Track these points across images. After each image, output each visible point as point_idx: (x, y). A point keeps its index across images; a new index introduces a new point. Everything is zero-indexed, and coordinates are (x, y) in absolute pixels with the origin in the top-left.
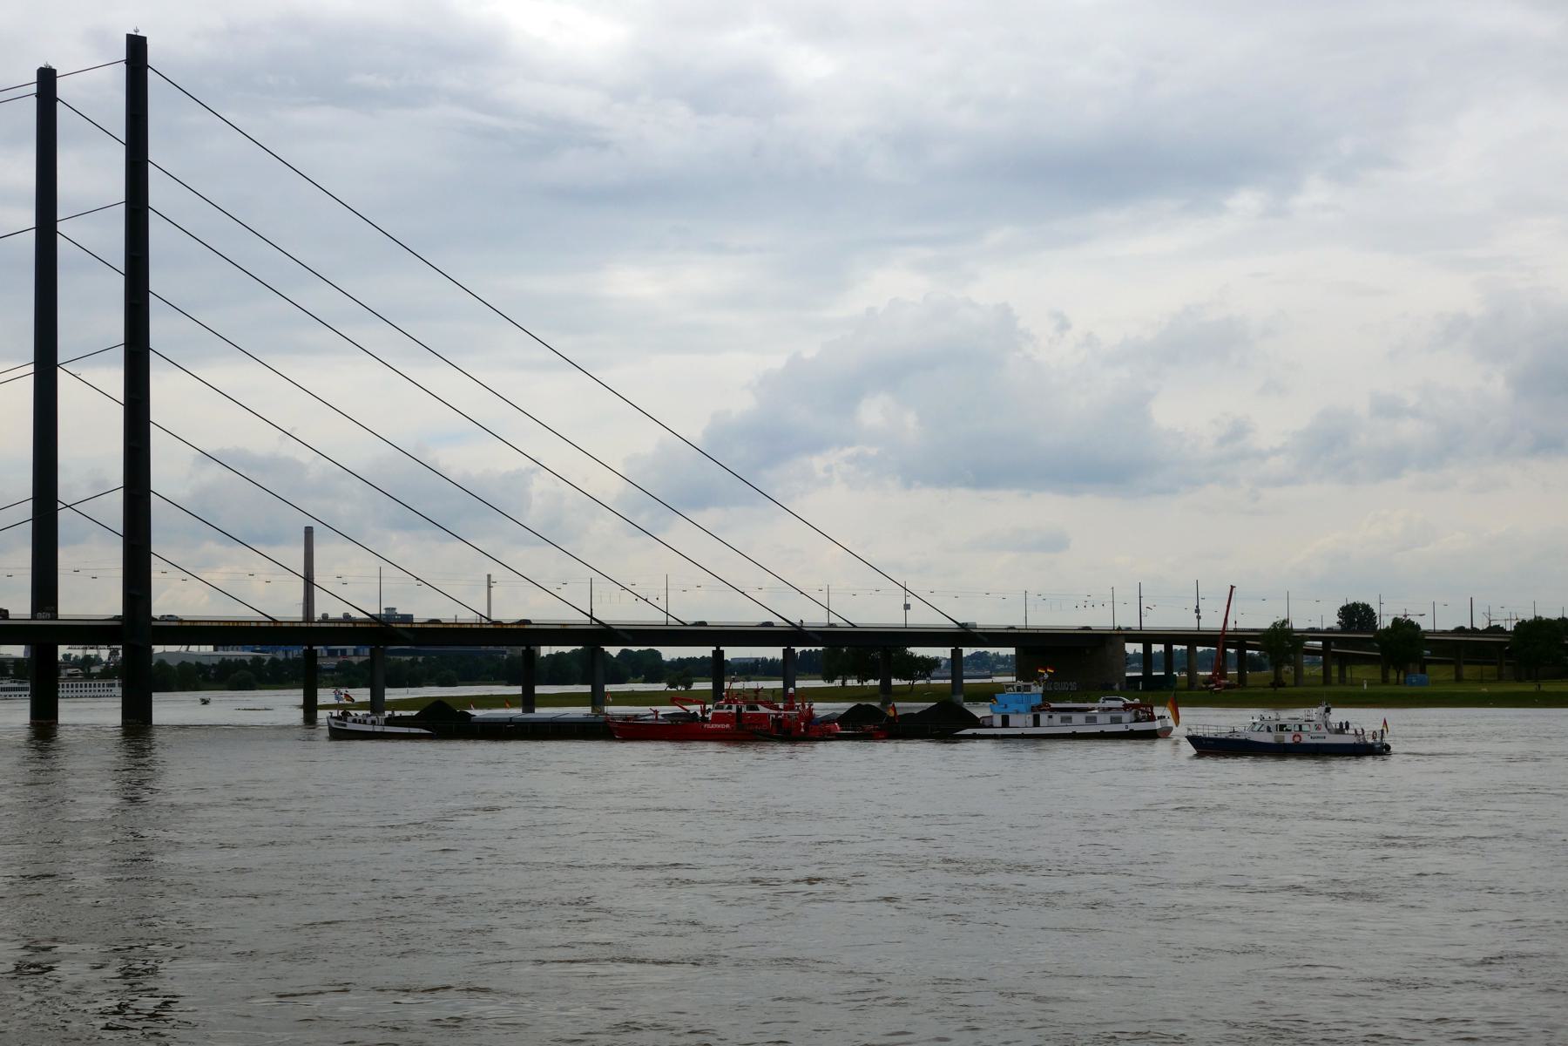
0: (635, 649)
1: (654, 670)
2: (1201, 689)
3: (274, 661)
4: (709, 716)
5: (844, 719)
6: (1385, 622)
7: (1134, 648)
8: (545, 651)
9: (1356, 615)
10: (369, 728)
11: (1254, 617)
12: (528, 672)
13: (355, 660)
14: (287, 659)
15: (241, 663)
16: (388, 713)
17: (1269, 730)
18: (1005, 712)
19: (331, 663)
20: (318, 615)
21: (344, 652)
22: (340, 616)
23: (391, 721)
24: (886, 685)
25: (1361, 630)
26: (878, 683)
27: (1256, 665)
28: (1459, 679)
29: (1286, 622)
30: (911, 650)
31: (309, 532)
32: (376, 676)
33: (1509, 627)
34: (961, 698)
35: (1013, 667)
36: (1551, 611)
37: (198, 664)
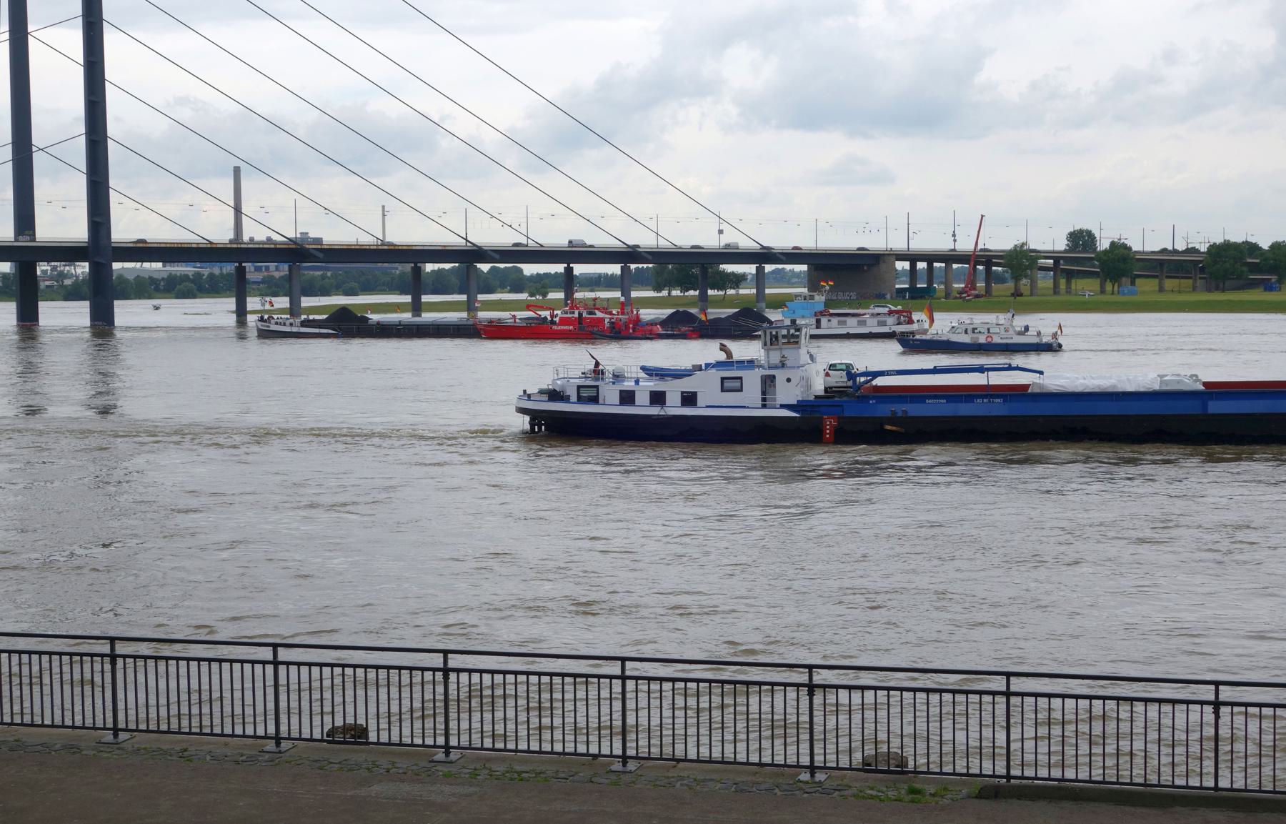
0: (502, 266)
1: (518, 283)
3: (211, 276)
4: (557, 319)
5: (664, 323)
6: (1103, 245)
7: (902, 265)
8: (429, 267)
9: (1081, 239)
10: (287, 329)
11: (1000, 241)
12: (416, 285)
13: (277, 275)
14: (222, 274)
15: (185, 278)
16: (303, 317)
17: (966, 332)
20: (246, 238)
21: (267, 268)
23: (305, 324)
24: (703, 297)
25: (1084, 251)
26: (697, 293)
27: (1000, 279)
28: (1161, 290)
29: (1023, 244)
30: (724, 267)
31: (237, 171)
33: (1265, 245)
34: (763, 305)
35: (806, 281)
36: (1280, 240)
37: (150, 278)
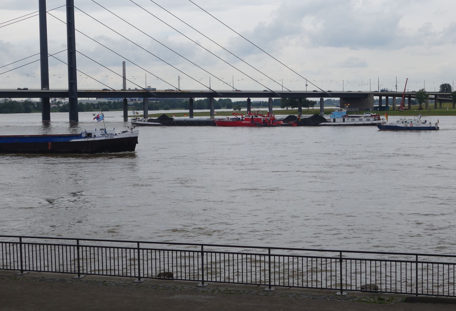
0: (223, 98)
1: (229, 105)
2: (397, 110)
3: (114, 103)
4: (244, 119)
5: (284, 120)
7: (376, 98)
8: (196, 99)
9: (446, 88)
10: (143, 123)
12: (191, 106)
13: (139, 102)
14: (118, 102)
15: (104, 103)
16: (149, 118)
18: (334, 117)
19: (132, 103)
20: (127, 89)
21: (135, 100)
22: (134, 89)
23: (149, 121)
24: (300, 110)
25: (447, 92)
26: (297, 109)
27: (414, 103)
31: (124, 63)
32: (145, 107)
34: (323, 113)
37: (92, 103)
